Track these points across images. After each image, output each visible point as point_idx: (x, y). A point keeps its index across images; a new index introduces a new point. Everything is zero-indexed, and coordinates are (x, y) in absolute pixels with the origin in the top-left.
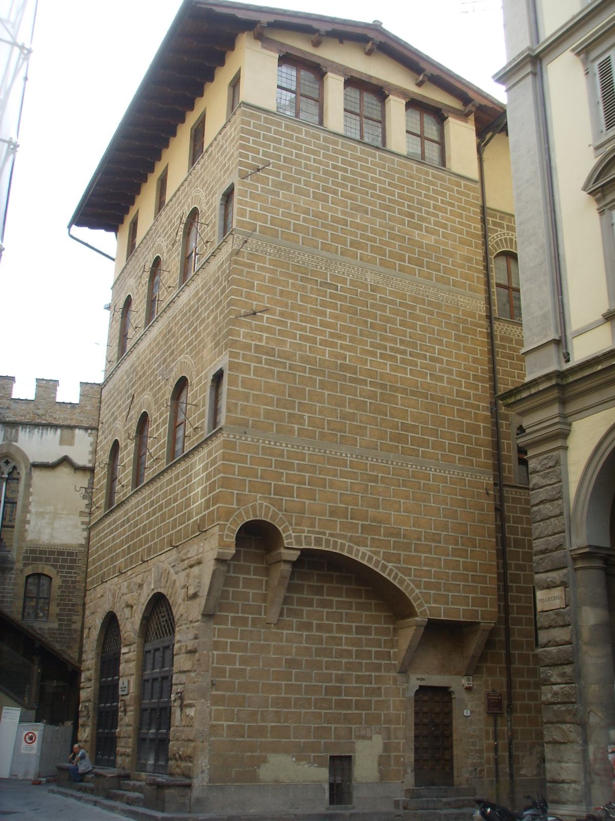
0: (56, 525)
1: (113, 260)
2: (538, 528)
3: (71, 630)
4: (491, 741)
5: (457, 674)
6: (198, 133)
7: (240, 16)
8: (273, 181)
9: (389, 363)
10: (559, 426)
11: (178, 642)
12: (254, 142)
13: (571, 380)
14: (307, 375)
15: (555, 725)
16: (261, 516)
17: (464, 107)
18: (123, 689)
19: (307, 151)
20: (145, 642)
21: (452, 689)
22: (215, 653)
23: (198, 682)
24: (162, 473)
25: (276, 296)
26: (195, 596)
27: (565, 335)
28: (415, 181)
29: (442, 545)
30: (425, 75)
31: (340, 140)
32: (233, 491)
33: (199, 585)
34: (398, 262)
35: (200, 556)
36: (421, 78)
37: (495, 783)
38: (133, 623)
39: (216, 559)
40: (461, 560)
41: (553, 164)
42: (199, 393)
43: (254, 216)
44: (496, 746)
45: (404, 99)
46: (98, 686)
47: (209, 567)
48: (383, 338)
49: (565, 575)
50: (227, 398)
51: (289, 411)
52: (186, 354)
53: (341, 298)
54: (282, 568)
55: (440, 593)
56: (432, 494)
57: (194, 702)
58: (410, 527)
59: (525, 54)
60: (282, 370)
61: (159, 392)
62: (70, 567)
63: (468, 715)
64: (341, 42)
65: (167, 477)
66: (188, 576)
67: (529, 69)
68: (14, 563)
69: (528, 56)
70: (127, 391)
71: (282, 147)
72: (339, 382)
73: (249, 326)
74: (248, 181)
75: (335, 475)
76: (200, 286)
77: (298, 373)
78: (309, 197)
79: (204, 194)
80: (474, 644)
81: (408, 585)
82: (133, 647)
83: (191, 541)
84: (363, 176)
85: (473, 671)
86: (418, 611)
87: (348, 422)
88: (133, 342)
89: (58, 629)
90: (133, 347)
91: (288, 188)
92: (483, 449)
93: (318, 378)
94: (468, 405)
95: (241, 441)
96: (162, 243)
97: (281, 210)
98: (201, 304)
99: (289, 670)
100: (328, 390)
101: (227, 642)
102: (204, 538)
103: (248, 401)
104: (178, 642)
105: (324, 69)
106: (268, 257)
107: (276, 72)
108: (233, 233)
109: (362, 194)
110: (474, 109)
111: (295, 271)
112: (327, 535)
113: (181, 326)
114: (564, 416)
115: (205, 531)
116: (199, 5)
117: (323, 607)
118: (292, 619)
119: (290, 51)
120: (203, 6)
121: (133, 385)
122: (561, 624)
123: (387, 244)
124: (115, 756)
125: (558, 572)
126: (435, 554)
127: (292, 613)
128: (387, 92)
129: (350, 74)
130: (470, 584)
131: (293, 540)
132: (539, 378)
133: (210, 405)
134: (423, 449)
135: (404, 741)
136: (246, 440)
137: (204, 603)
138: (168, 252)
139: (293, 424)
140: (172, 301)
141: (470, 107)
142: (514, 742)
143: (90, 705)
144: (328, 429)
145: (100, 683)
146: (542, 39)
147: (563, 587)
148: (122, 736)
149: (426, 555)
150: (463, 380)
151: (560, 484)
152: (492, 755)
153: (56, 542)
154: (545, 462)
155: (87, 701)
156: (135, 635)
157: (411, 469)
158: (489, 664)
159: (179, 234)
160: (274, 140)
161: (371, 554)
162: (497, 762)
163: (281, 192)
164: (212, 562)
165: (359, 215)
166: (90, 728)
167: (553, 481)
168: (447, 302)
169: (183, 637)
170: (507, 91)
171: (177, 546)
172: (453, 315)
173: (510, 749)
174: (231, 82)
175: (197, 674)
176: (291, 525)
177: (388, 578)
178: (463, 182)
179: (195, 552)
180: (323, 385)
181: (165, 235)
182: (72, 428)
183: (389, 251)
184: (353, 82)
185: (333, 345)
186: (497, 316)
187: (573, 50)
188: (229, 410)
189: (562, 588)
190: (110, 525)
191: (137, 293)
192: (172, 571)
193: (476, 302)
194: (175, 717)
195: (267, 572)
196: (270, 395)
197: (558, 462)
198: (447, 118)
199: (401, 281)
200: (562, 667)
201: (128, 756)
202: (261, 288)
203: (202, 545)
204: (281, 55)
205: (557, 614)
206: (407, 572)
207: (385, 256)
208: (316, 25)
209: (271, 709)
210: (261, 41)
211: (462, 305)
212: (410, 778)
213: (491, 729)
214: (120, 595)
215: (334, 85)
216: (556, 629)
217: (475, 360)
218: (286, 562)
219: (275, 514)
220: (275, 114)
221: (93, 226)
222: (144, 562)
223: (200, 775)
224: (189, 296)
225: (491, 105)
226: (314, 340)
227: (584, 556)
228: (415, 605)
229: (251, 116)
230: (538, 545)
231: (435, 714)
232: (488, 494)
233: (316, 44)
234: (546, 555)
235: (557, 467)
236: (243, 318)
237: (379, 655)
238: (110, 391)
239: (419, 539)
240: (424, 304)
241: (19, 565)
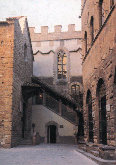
68: (67, 82)
124: (93, 139)
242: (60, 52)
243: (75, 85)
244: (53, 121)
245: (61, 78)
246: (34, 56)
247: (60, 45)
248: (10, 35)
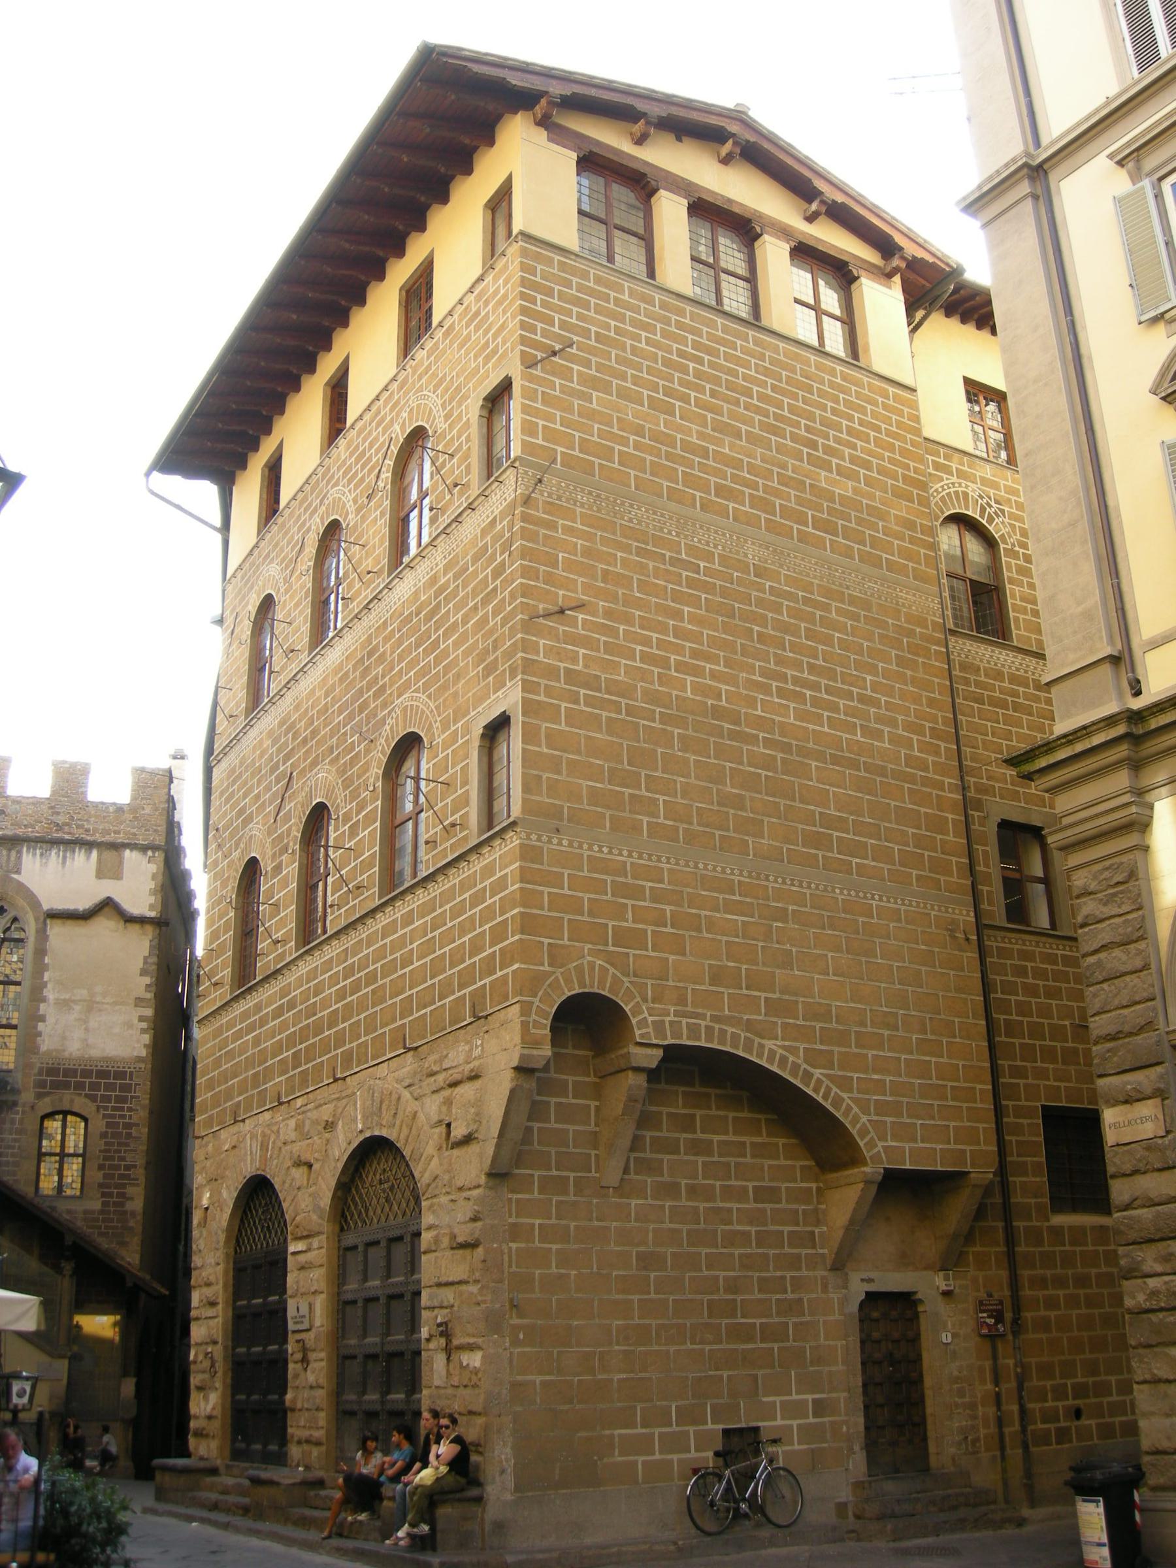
0: (93, 1024)
2: (1097, 996)
3: (125, 1212)
4: (989, 1386)
5: (926, 1268)
6: (418, 294)
8: (580, 374)
9: (792, 705)
11: (430, 1228)
12: (545, 304)
13: (1154, 724)
14: (657, 725)
15: (1155, 1349)
16: (592, 987)
18: (299, 1319)
19: (634, 323)
20: (342, 1230)
22: (514, 1245)
23: (485, 1302)
24: (373, 912)
25: (596, 581)
26: (468, 1140)
27: (1130, 649)
28: (815, 385)
29: (900, 1033)
30: (823, 202)
32: (542, 939)
33: (478, 1118)
34: (795, 526)
35: (476, 1063)
36: (814, 206)
37: (999, 1460)
39: (517, 1069)
40: (933, 1059)
41: (1083, 350)
42: (451, 758)
43: (549, 434)
44: (998, 1395)
46: (230, 1314)
48: (780, 661)
49: (1161, 1077)
50: (523, 767)
51: (631, 791)
52: (416, 691)
53: (708, 588)
54: (630, 1082)
55: (902, 1120)
56: (878, 941)
57: (480, 1341)
58: (847, 1002)
59: (1020, 163)
60: (613, 715)
61: (352, 766)
62: (123, 1100)
63: (950, 1340)
64: (679, 139)
65: (382, 920)
66: (448, 1102)
67: (1025, 188)
69: (1026, 165)
70: (274, 769)
71: (592, 314)
72: (712, 739)
73: (552, 634)
74: (537, 372)
75: (717, 910)
76: (441, 566)
77: (642, 722)
78: (643, 405)
79: (439, 402)
81: (849, 1109)
83: (450, 1037)
84: (730, 372)
85: (950, 1261)
86: (867, 1155)
87: (732, 811)
88: (284, 678)
89: (102, 1212)
90: (285, 686)
91: (606, 388)
92: (954, 859)
93: (676, 731)
94: (926, 781)
95: (551, 846)
96: (343, 499)
97: (596, 426)
98: (473, 590)
99: (644, 1273)
100: (694, 753)
101: (534, 1225)
102: (485, 1029)
103: (559, 773)
104: (430, 1228)
105: (653, 183)
106: (579, 510)
107: (576, 186)
108: (517, 464)
109: (729, 403)
110: (903, 265)
111: (626, 537)
112: (708, 1018)
113: (400, 642)
115: (486, 1017)
117: (696, 1154)
118: (645, 1178)
121: (287, 757)
122: (1158, 1165)
125: (1146, 1072)
126: (889, 1051)
127: (648, 1167)
128: (758, 229)
129: (697, 195)
130: (951, 1103)
131: (650, 1030)
132: (1094, 724)
133: (479, 782)
134: (605, 897)
135: (846, 1394)
137: (491, 1153)
138: (358, 511)
139: (639, 814)
140: (375, 597)
141: (896, 262)
142: (1026, 1385)
143: (218, 1351)
144: (699, 825)
145: (234, 1309)
146: (1045, 141)
147: (1158, 1100)
148: (299, 1406)
149: (875, 1052)
150: (915, 737)
151: (1140, 913)
152: (991, 1411)
153: (95, 1053)
154: (1106, 874)
155: (207, 1343)
156: (321, 1218)
157: (840, 897)
158: (978, 1249)
159: (383, 476)
160: (577, 302)
161: (784, 1053)
162: (1000, 1423)
163: (595, 394)
164: (509, 1075)
165: (727, 440)
166: (219, 1392)
167: (1125, 908)
168: (879, 598)
170: (985, 225)
171: (417, 1048)
172: (890, 621)
173: (1021, 1398)
174: (489, 201)
175: (482, 1287)
176: (645, 1000)
177: (815, 1096)
178: (891, 390)
179: (462, 1058)
180: (686, 746)
181: (349, 482)
182: (117, 847)
183: (781, 505)
184: (707, 211)
185: (697, 671)
186: (952, 627)
188: (526, 789)
190: (245, 1015)
191: (287, 592)
192: (406, 1094)
193: (927, 599)
194: (432, 1369)
195: (597, 1092)
196: (597, 762)
197: (1132, 875)
198: (858, 278)
199: (803, 559)
200: (1164, 1243)
201: (318, 1444)
202: (569, 566)
203: (479, 1042)
206: (844, 1084)
207: (774, 514)
208: (641, 106)
209: (616, 1348)
210: (546, 129)
211: (903, 605)
212: (857, 1463)
213: (988, 1364)
214: (279, 1144)
215: (670, 212)
216: (1148, 1176)
217: (931, 702)
219: (616, 981)
220: (577, 255)
222: (336, 1080)
223: (497, 1479)
224: (415, 585)
225: (931, 260)
226: (664, 663)
228: (861, 1144)
229: (537, 257)
230: (1099, 1025)
231: (893, 1342)
232: (967, 939)
233: (640, 141)
234: (1120, 1042)
236: (541, 620)
237: (797, 1239)
238: (233, 771)
239: (862, 1023)
240: (843, 602)
241: (27, 1097)
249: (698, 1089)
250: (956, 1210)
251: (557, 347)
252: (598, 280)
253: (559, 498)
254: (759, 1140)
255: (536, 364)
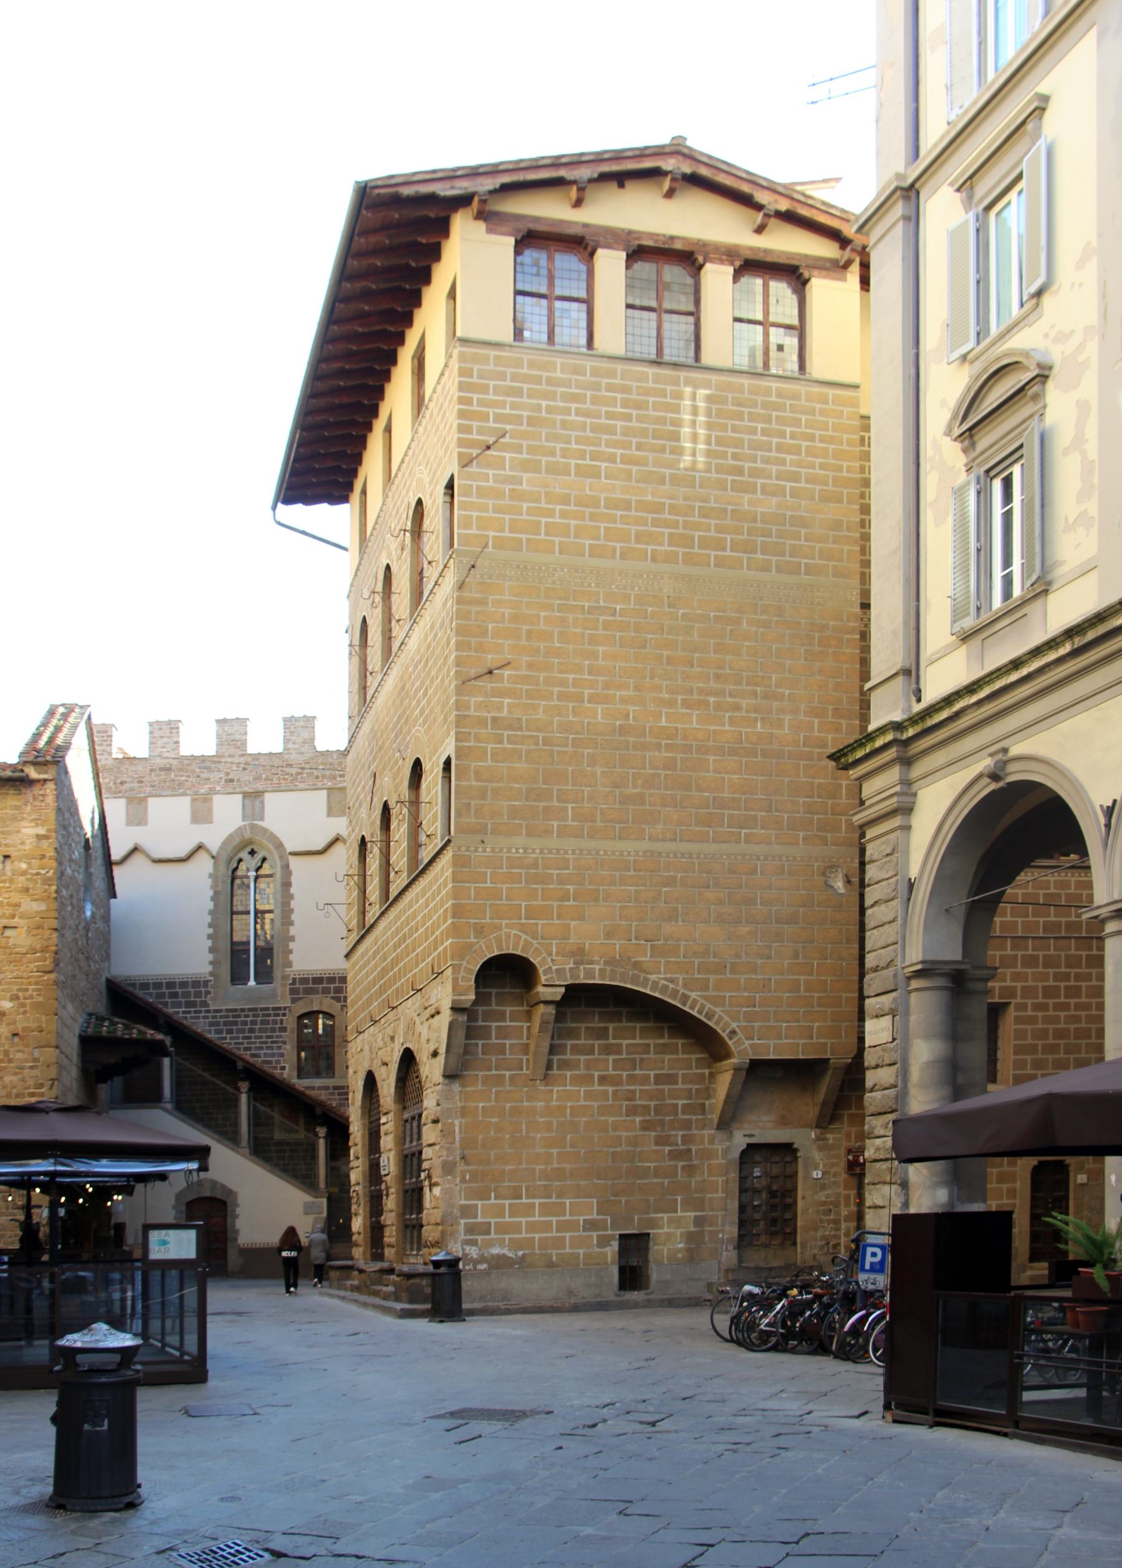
1: (346, 549)
7: (442, 194)
10: (895, 799)
17: (841, 252)
21: (795, 1146)
31: (620, 367)
38: (388, 1085)
45: (732, 263)
47: (446, 1017)
49: (895, 999)
59: (892, 187)
74: (473, 469)
80: (825, 1086)
82: (391, 1116)
114: (906, 783)
116: (377, 191)
119: (532, 226)
120: (382, 191)
121: (374, 759)
123: (696, 527)
124: (383, 1248)
129: (637, 242)
136: (484, 851)
150: (816, 721)
154: (883, 847)
169: (430, 1102)
184: (640, 252)
187: (951, 184)
189: (889, 1017)
190: (363, 955)
195: (529, 1016)
204: (519, 238)
205: (883, 1050)
206: (718, 1001)
215: (610, 264)
218: (546, 1002)
219: (528, 944)
220: (511, 346)
221: (309, 499)
227: (918, 974)
231: (772, 1177)
233: (578, 203)
235: (899, 852)
242: (244, 854)
243: (313, 1015)
244: (212, 1181)
245: (248, 980)
246: (117, 872)
247: (244, 820)
248: (42, 831)
249: (612, 1009)
250: (825, 1086)
251: (491, 440)
252: (532, 365)
253: (490, 577)
254: (662, 1041)
255: (471, 461)
